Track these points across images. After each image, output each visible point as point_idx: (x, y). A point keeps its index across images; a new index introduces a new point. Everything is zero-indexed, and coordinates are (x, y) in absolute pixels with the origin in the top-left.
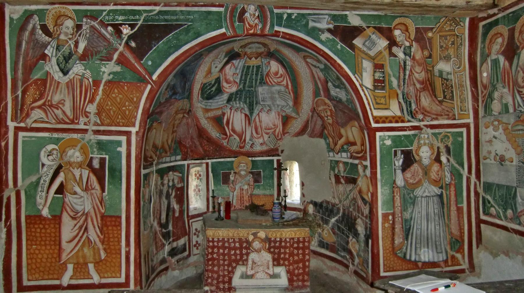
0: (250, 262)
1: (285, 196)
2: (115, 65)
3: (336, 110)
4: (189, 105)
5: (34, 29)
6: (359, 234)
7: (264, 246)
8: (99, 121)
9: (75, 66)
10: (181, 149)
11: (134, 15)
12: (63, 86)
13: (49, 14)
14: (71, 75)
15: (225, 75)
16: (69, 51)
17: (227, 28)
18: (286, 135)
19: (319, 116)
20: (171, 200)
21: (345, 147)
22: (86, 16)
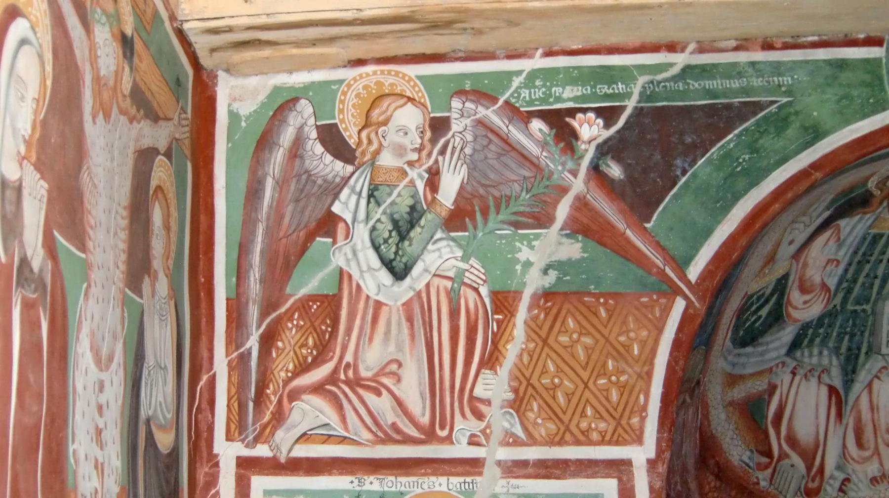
2: (564, 240)
5: (299, 142)
8: (519, 431)
9: (430, 247)
11: (611, 82)
12: (393, 314)
13: (344, 93)
14: (418, 278)
16: (410, 202)
22: (461, 93)
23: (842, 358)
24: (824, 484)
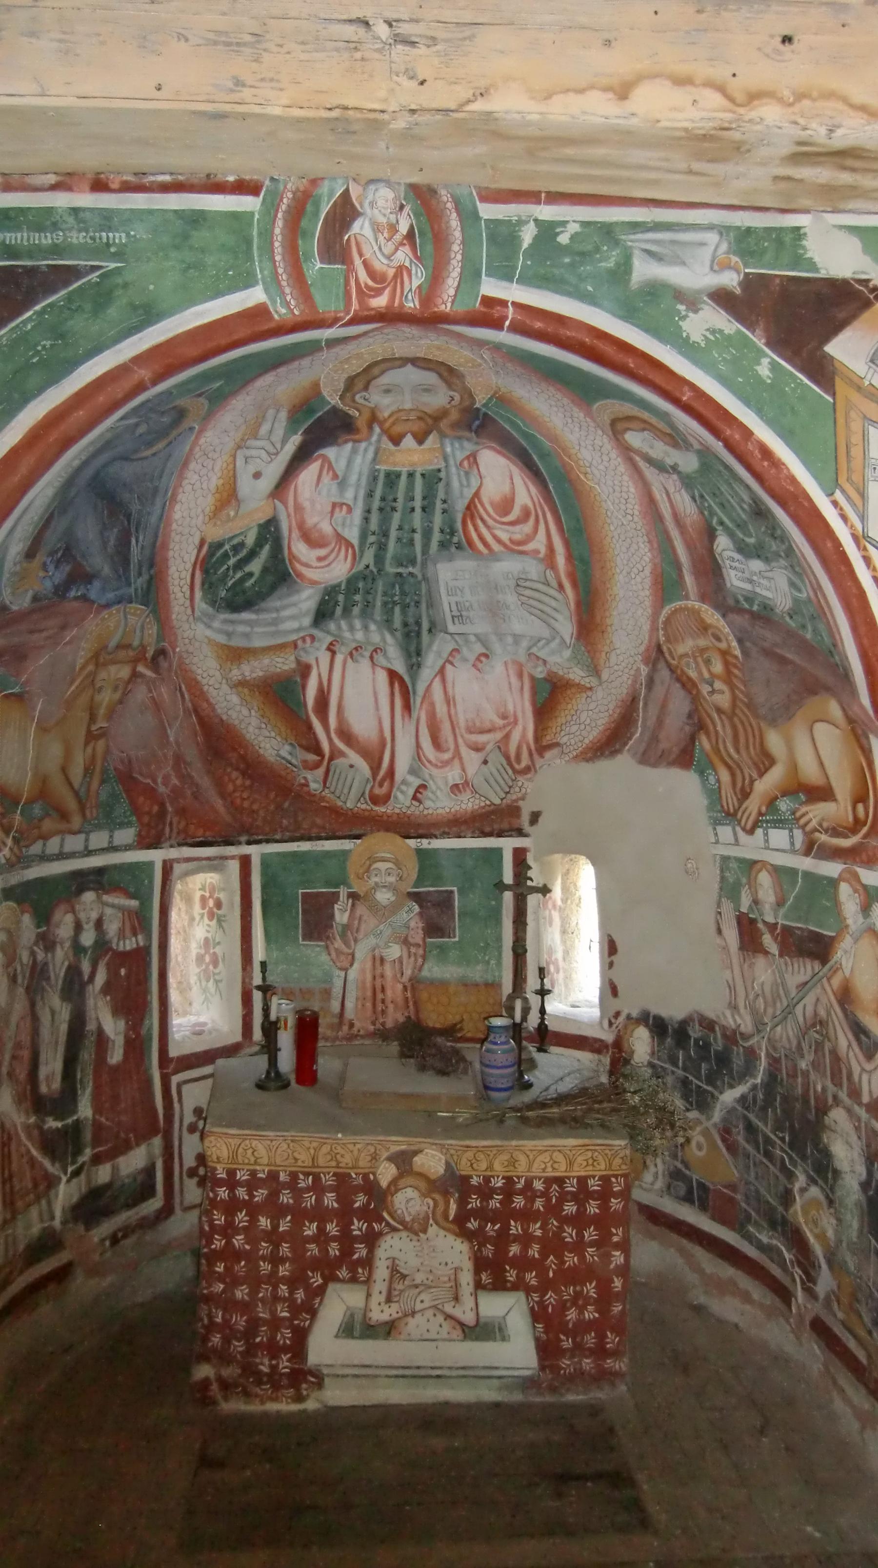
0: (381, 1272)
1: (543, 992)
3: (745, 652)
4: (153, 630)
6: (836, 1173)
7: (441, 1207)
10: (133, 803)
15: (298, 508)
17: (273, 284)
18: (548, 755)
19: (678, 680)
20: (90, 1002)
21: (784, 805)
23: (398, 634)
24: (395, 790)
